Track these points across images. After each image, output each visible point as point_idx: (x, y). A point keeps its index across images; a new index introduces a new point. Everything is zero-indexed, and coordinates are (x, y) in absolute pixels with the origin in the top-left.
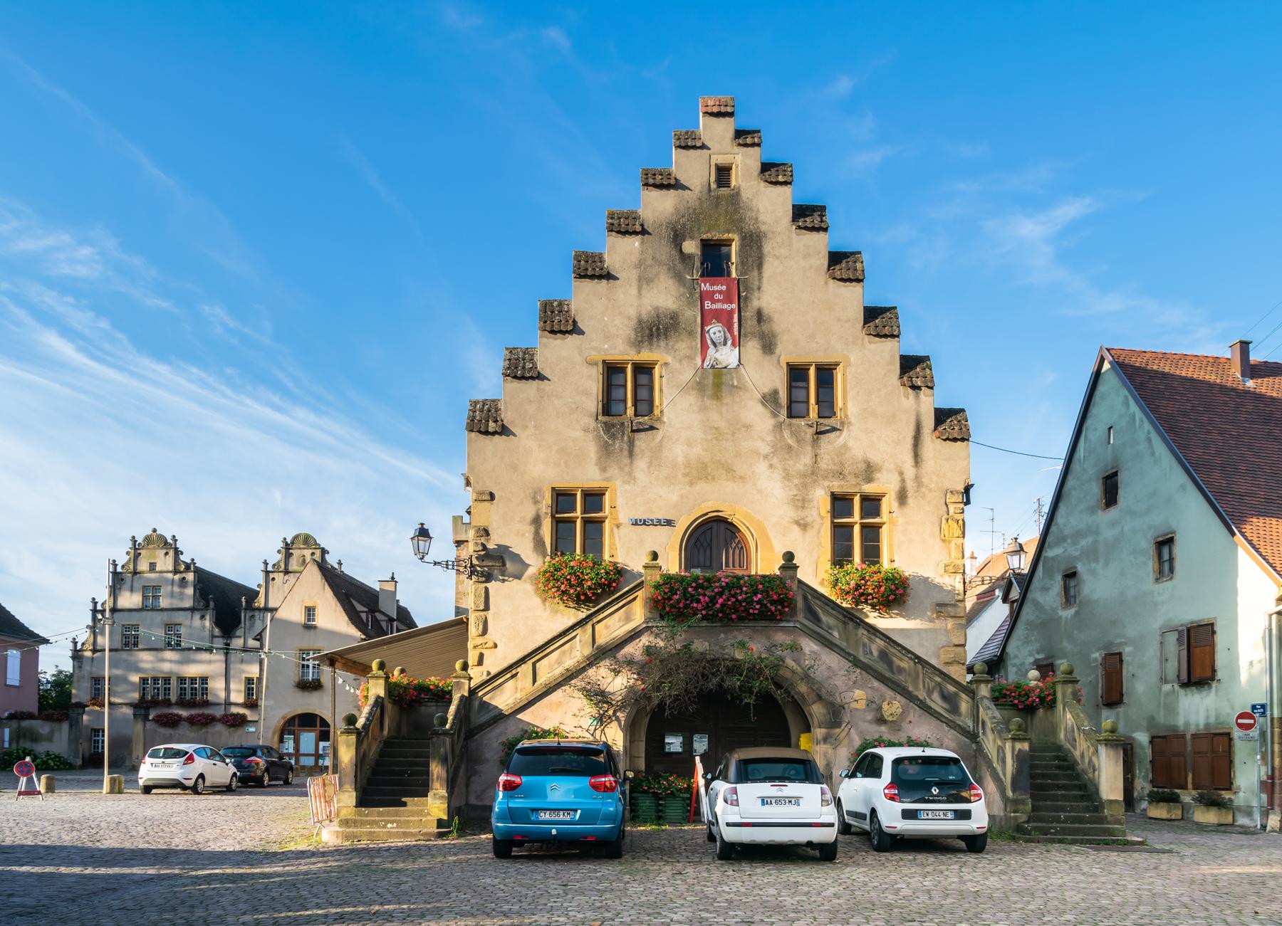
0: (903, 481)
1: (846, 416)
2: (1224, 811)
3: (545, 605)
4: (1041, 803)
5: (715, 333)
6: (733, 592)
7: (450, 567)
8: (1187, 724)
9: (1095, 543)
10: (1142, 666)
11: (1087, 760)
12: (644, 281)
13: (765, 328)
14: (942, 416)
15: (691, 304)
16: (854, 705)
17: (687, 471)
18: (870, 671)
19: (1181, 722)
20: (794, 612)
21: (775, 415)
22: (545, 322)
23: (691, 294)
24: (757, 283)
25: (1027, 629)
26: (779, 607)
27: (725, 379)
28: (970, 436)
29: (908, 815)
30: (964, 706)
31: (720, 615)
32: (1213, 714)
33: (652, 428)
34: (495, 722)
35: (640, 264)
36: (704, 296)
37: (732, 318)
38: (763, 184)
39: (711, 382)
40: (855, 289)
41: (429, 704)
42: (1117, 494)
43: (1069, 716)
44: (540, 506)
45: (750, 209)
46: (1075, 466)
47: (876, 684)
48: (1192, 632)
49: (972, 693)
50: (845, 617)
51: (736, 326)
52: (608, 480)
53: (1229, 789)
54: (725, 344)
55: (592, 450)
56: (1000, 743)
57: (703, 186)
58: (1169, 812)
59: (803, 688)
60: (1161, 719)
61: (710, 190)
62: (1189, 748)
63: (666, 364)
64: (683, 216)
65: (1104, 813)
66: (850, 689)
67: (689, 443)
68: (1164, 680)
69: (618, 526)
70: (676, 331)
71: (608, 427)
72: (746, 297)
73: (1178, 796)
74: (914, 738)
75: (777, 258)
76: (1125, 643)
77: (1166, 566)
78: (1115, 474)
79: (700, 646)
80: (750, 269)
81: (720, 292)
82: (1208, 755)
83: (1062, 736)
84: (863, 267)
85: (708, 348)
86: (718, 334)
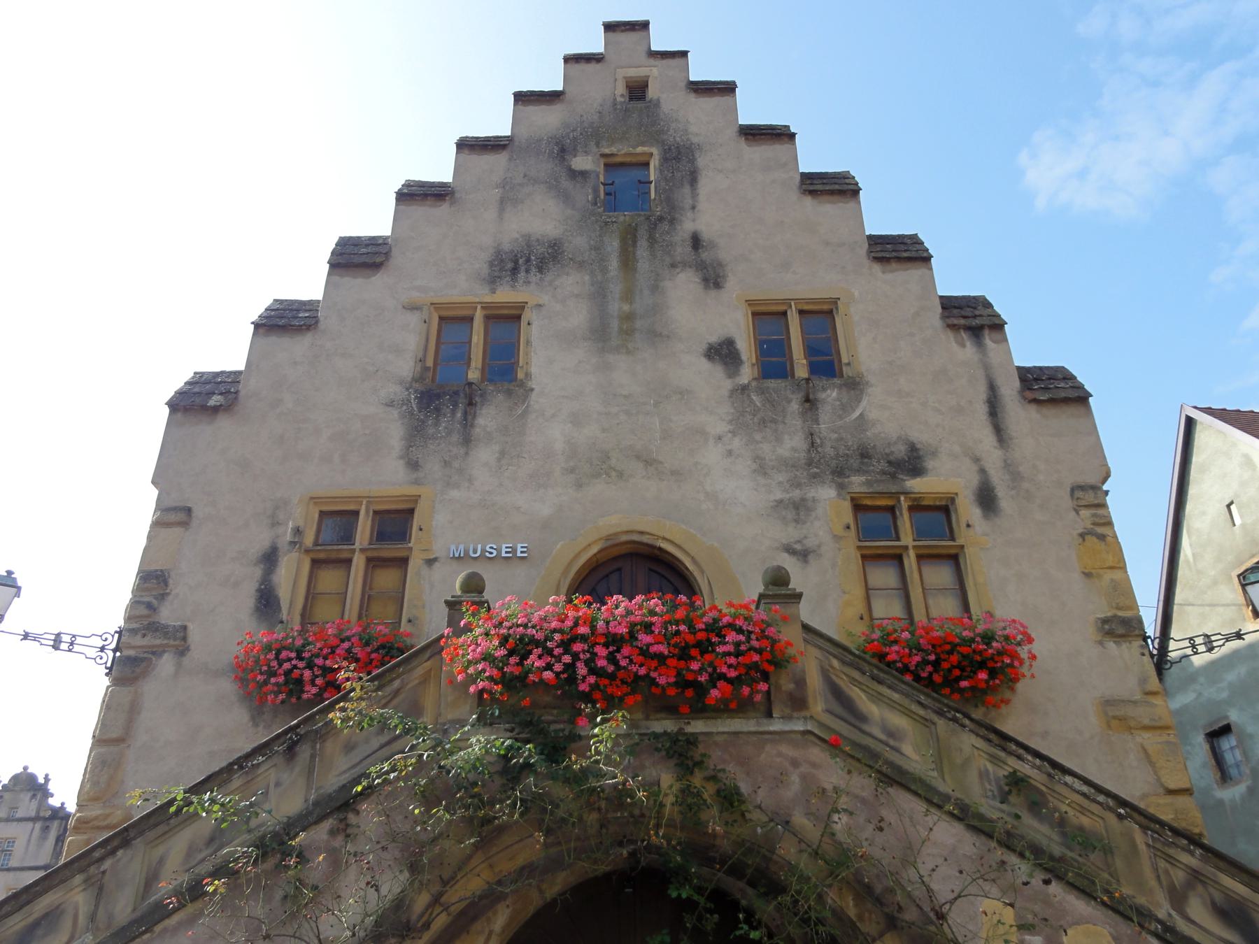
13: (704, 255)
17: (572, 464)
24: (691, 202)
67: (576, 420)
75: (720, 171)
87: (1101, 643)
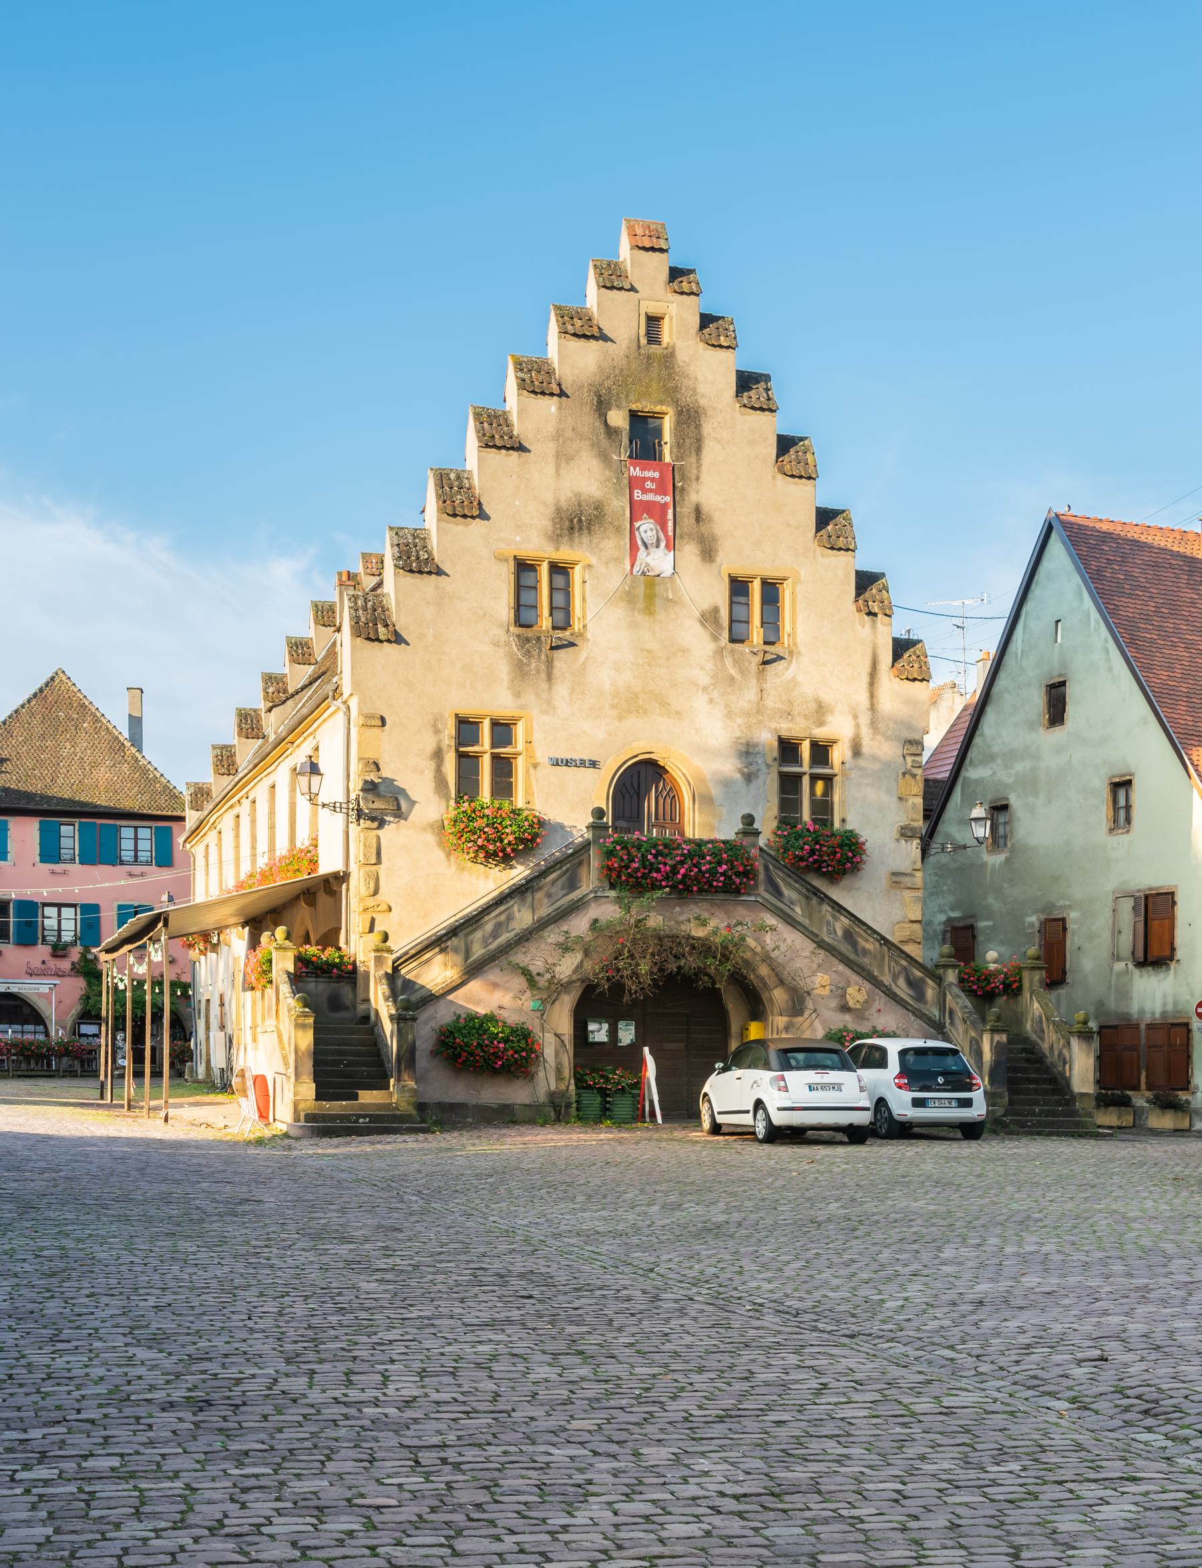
0: (858, 726)
1: (795, 644)
2: (1180, 1114)
3: (449, 860)
4: (1015, 1097)
5: (646, 532)
6: (695, 861)
7: (338, 810)
8: (1142, 1012)
9: (1034, 770)
10: (1091, 937)
11: (1056, 1053)
12: (563, 458)
13: (704, 528)
14: (901, 647)
15: (618, 492)
16: (820, 991)
18: (835, 953)
19: (1134, 1009)
20: (756, 886)
21: (715, 638)
22: (444, 502)
23: (618, 479)
25: (936, 875)
26: (745, 880)
27: (659, 589)
28: (930, 677)
29: (918, 1103)
30: (930, 993)
31: (681, 887)
32: (1170, 1000)
33: (572, 644)
34: (424, 1005)
35: (558, 436)
36: (635, 483)
37: (666, 513)
38: (702, 345)
39: (642, 593)
40: (804, 486)
41: (307, 979)
42: (1064, 711)
43: (1036, 1005)
44: (442, 736)
45: (687, 376)
46: (1009, 660)
47: (841, 967)
48: (1150, 900)
49: (939, 980)
50: (808, 890)
51: (670, 524)
52: (522, 707)
53: (1187, 1089)
54: (658, 546)
55: (504, 670)
56: (973, 1034)
57: (631, 341)
58: (1119, 1117)
59: (764, 971)
60: (1112, 1005)
61: (639, 347)
62: (1143, 1041)
63: (590, 566)
64: (608, 378)
65: (1075, 1106)
66: (814, 974)
68: (1116, 957)
69: (535, 766)
70: (601, 525)
71: (523, 641)
72: (683, 489)
73: (1129, 1099)
74: (879, 1028)
76: (1070, 907)
77: (1122, 813)
78: (1063, 684)
79: (655, 921)
80: (688, 453)
81: (653, 480)
82: (1165, 1049)
83: (1029, 1027)
84: (815, 460)
85: (638, 549)
86: (649, 533)
87: (897, 840)
